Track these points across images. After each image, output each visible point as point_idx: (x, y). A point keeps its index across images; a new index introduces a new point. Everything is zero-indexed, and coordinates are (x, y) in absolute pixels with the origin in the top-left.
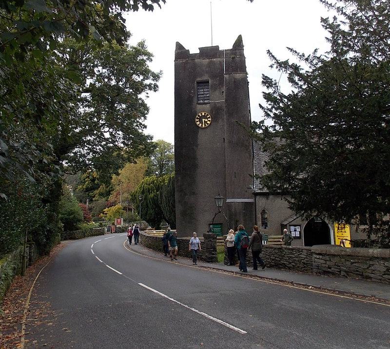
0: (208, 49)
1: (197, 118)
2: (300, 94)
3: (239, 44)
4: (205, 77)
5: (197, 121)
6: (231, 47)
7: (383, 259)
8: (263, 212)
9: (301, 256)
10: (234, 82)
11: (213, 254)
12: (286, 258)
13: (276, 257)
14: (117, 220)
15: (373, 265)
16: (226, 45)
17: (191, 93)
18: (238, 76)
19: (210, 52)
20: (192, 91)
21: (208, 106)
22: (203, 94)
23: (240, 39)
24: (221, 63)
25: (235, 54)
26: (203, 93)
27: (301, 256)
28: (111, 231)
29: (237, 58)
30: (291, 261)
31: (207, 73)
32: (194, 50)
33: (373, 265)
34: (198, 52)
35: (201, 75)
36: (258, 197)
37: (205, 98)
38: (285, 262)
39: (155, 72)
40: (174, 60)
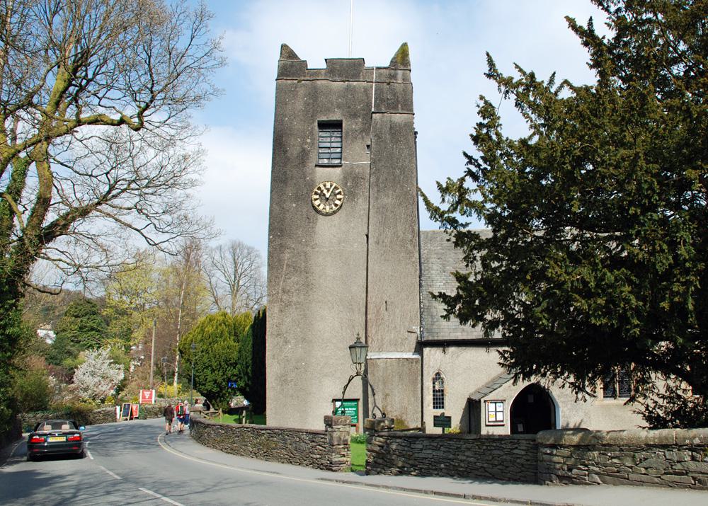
0: (342, 65)
1: (316, 193)
2: (32, 320)
3: (402, 58)
4: (335, 116)
5: (316, 199)
6: (387, 64)
7: (665, 447)
8: (438, 377)
9: (515, 451)
10: (391, 128)
11: (344, 456)
12: (487, 458)
13: (468, 457)
14: (143, 394)
15: (645, 459)
16: (378, 57)
17: (307, 143)
18: (398, 118)
19: (347, 69)
20: (309, 141)
21: (338, 170)
22: (329, 148)
23: (405, 45)
24: (366, 91)
25: (394, 77)
26: (328, 145)
27: (515, 451)
28: (132, 414)
29: (398, 86)
30: (496, 463)
31: (338, 107)
32: (316, 62)
33: (645, 459)
34: (324, 66)
35: (328, 110)
36: (426, 351)
37: (333, 156)
38: (485, 465)
39: (577, 23)
40: (276, 77)
